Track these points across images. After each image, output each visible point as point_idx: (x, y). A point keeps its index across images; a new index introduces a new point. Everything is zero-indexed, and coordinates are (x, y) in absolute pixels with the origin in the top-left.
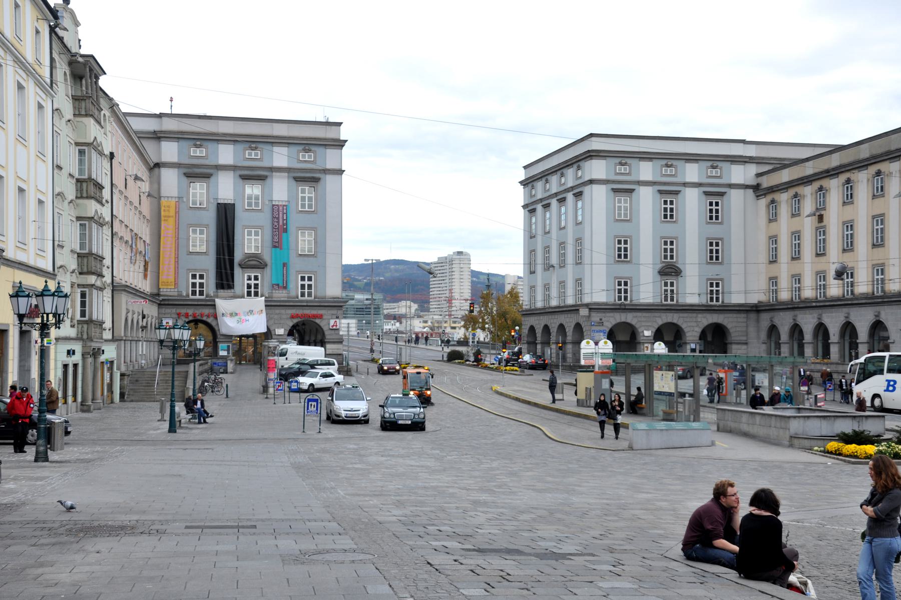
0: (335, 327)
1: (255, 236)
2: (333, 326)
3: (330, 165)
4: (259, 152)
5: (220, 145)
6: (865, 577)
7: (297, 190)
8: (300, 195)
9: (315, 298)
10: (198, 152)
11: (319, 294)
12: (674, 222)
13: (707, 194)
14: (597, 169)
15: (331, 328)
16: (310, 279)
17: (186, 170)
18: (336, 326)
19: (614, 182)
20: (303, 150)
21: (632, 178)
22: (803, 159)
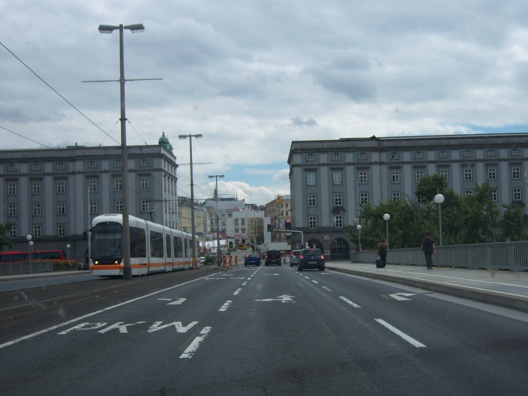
0: (327, 240)
1: (311, 200)
2: (326, 239)
3: (155, 167)
4: (339, 156)
5: (346, 154)
6: (96, 325)
7: (391, 173)
8: (142, 182)
9: (343, 227)
10: (443, 155)
11: (319, 226)
12: (399, 183)
13: (358, 168)
14: (79, 166)
15: (325, 240)
16: (314, 219)
17: (389, 165)
18: (327, 239)
19: (87, 172)
20: (441, 152)
21: (369, 161)
22: (174, 155)
